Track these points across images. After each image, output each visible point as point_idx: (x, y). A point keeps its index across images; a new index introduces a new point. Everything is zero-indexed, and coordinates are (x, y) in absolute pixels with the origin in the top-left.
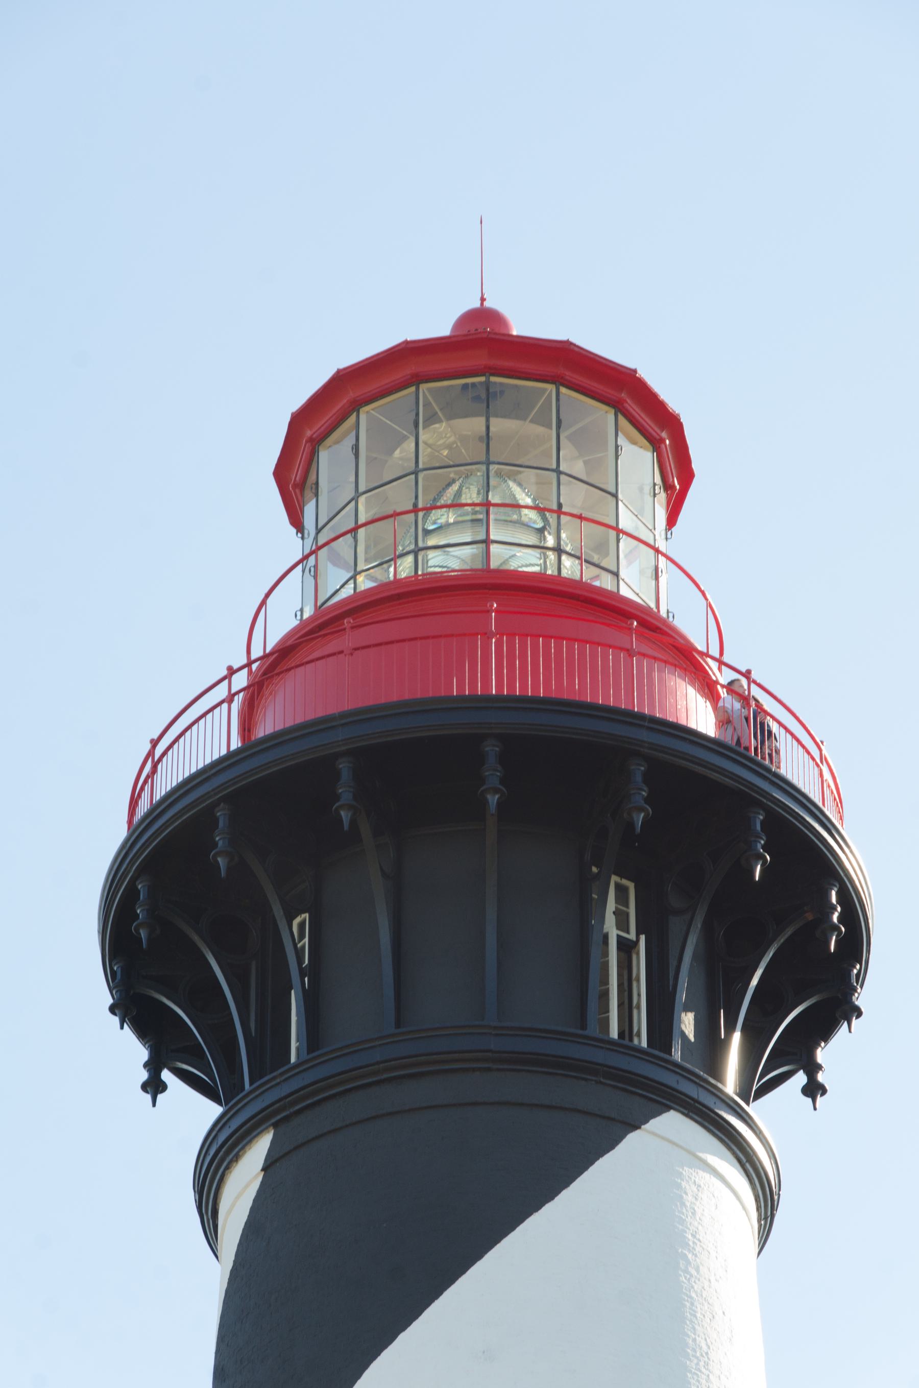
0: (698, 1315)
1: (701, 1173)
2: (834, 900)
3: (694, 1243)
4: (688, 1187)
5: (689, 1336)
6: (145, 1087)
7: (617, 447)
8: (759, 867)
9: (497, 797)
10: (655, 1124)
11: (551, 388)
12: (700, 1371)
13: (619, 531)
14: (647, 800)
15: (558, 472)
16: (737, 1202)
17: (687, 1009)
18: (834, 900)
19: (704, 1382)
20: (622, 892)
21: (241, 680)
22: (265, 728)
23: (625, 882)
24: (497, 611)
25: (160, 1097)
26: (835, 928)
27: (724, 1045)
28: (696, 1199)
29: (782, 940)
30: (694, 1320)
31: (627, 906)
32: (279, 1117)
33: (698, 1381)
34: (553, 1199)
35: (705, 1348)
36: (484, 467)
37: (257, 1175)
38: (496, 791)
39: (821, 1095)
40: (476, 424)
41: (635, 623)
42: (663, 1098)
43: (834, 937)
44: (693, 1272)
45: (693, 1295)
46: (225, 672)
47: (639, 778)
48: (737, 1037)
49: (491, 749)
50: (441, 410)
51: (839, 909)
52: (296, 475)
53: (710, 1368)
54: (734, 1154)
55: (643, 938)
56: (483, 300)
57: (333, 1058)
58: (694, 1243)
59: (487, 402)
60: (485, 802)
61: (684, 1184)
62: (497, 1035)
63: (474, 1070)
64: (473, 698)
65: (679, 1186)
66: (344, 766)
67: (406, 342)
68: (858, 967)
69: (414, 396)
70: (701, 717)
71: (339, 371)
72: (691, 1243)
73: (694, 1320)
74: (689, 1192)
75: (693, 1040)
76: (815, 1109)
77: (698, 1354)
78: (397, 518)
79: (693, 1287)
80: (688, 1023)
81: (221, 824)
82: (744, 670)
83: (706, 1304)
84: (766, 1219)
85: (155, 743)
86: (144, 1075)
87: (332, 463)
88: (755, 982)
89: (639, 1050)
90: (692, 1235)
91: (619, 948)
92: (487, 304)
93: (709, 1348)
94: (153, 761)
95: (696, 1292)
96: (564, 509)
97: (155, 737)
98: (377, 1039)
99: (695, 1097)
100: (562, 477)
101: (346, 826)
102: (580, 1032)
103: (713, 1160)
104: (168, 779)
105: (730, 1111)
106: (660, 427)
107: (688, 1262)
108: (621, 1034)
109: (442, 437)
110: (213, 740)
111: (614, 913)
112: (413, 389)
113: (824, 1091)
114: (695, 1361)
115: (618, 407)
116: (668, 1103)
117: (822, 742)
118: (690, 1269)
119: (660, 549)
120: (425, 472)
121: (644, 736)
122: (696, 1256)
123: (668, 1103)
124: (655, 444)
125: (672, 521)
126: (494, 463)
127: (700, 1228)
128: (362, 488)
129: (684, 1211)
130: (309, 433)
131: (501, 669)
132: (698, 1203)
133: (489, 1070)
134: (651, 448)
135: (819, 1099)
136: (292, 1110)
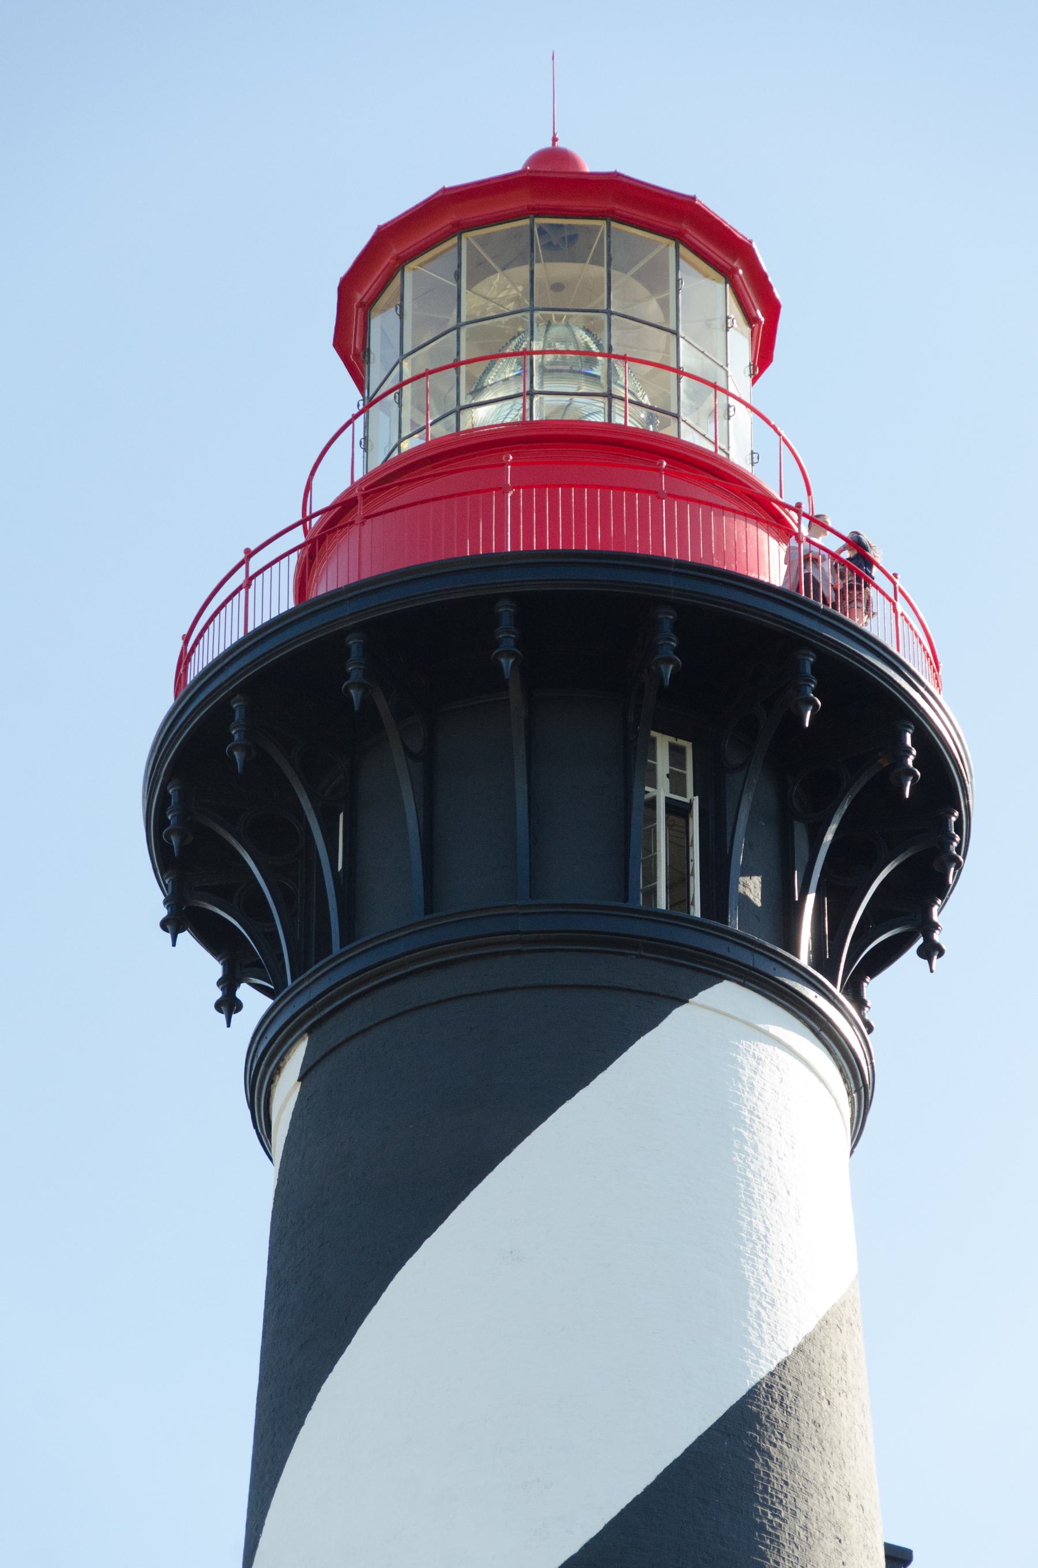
0: (756, 1196)
1: (762, 1045)
2: (909, 742)
3: (751, 1119)
4: (745, 1061)
5: (743, 1219)
6: (218, 1006)
7: (677, 280)
8: (809, 713)
9: (511, 661)
10: (705, 997)
11: (602, 224)
12: (757, 1256)
13: (679, 372)
14: (676, 651)
15: (609, 313)
16: (812, 1075)
17: (748, 872)
18: (909, 742)
19: (761, 1267)
20: (676, 755)
23: (681, 742)
24: (512, 464)
25: (234, 1016)
26: (910, 772)
28: (756, 1073)
29: (856, 790)
30: (750, 1201)
31: (684, 767)
32: (310, 1023)
33: (754, 1266)
34: (587, 1084)
35: (762, 1230)
36: (528, 315)
37: (294, 1088)
38: (510, 654)
39: (939, 957)
41: (665, 464)
42: (696, 962)
43: (909, 783)
44: (751, 1151)
45: (750, 1175)
46: (242, 556)
47: (667, 627)
48: (811, 898)
49: (505, 610)
50: (492, 258)
51: (914, 752)
52: (356, 343)
53: (769, 1252)
54: (805, 1022)
55: (697, 798)
56: (555, 140)
57: (362, 952)
58: (751, 1119)
59: (564, 247)
60: (499, 669)
61: (740, 1058)
62: (524, 914)
63: (504, 953)
64: (488, 556)
65: (734, 1061)
66: (353, 642)
67: (444, 190)
68: (957, 814)
69: (456, 250)
70: (771, 563)
71: (379, 228)
72: (748, 1121)
73: (750, 1201)
74: (747, 1066)
75: (759, 904)
76: (932, 971)
77: (754, 1238)
78: (430, 377)
79: (749, 1167)
80: (752, 888)
81: (237, 717)
82: (793, 505)
83: (765, 1184)
84: (858, 1091)
85: (186, 639)
86: (218, 994)
87: (382, 326)
88: (829, 837)
89: (694, 921)
90: (749, 1111)
91: (668, 811)
92: (560, 144)
93: (768, 1230)
94: (184, 660)
95: (753, 1172)
96: (613, 353)
97: (186, 632)
98: (399, 930)
99: (750, 963)
100: (613, 317)
101: (356, 706)
102: (622, 904)
103: (773, 1030)
104: (195, 669)
105: (794, 976)
106: (726, 252)
107: (745, 1141)
108: (672, 902)
109: (500, 290)
110: (275, 597)
111: (668, 776)
112: (455, 240)
113: (941, 952)
114: (751, 1245)
115: (678, 237)
116: (719, 972)
117: (895, 575)
118: (746, 1148)
119: (718, 384)
120: (468, 326)
121: (671, 582)
122: (754, 1133)
123: (719, 972)
124: (728, 275)
125: (763, 357)
126: (539, 309)
127: (760, 1103)
128: (407, 349)
129: (740, 1086)
130: (359, 296)
131: (512, 524)
132: (757, 1077)
133: (519, 952)
134: (723, 280)
135: (935, 960)
136: (323, 1013)
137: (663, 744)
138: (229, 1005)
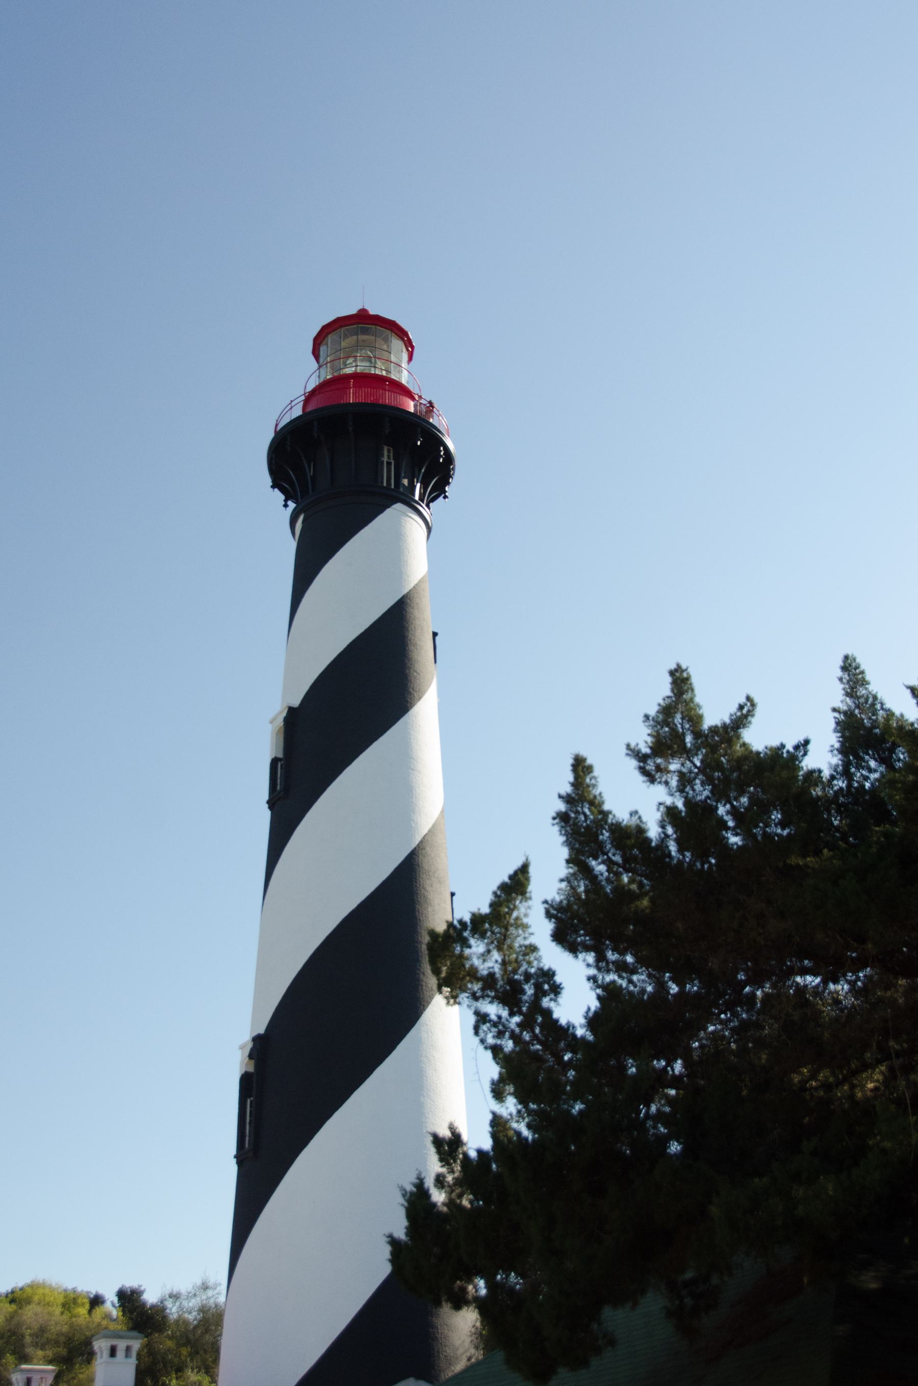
20: (389, 451)
21: (303, 398)
22: (309, 409)
27: (415, 487)
40: (355, 337)
70: (411, 407)
80: (405, 482)
87: (323, 349)
94: (277, 425)
104: (278, 429)
106: (402, 334)
110: (298, 412)
137: (386, 448)
138: (286, 506)
